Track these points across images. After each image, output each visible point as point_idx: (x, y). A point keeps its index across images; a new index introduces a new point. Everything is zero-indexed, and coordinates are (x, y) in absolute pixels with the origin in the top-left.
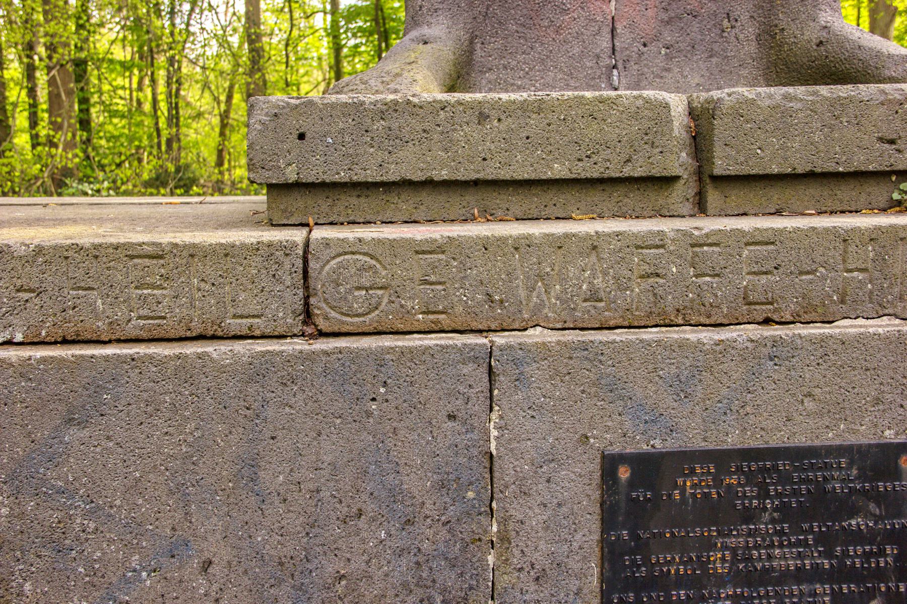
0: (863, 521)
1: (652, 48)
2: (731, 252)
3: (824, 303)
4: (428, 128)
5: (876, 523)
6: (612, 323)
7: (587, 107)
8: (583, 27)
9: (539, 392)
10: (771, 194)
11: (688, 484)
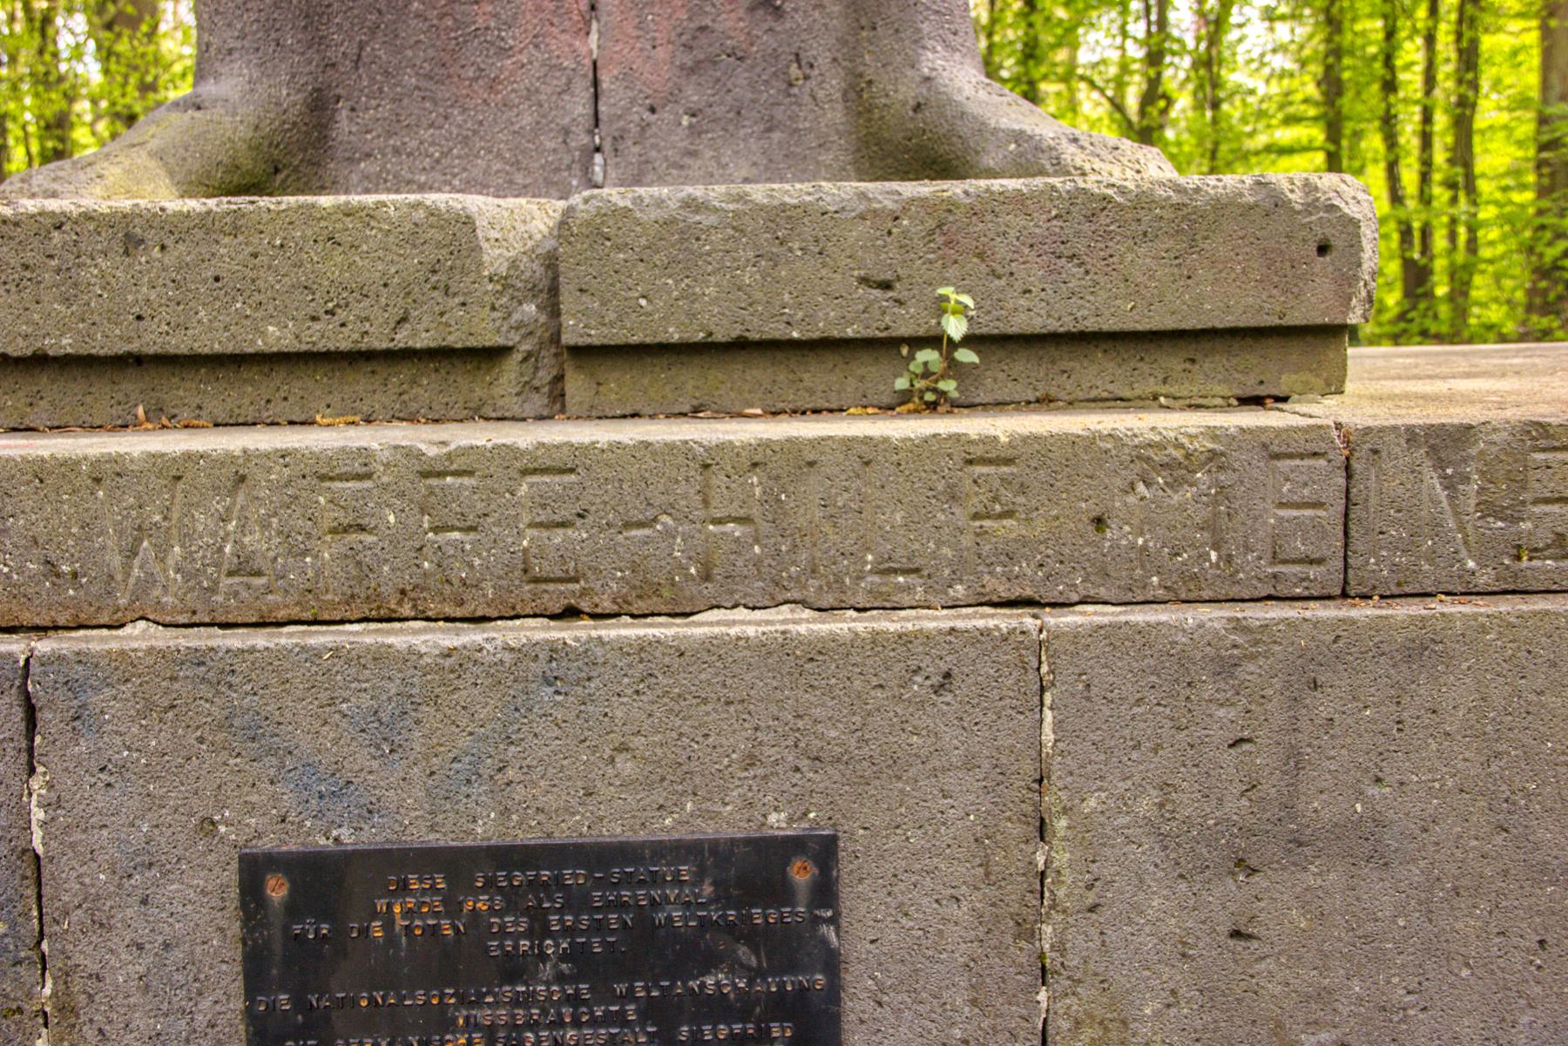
0: (727, 978)
1: (666, 115)
2: (496, 486)
3: (673, 579)
4: (31, 262)
5: (751, 983)
6: (281, 615)
7: (323, 224)
8: (538, 79)
9: (118, 740)
10: (682, 378)
11: (397, 909)
